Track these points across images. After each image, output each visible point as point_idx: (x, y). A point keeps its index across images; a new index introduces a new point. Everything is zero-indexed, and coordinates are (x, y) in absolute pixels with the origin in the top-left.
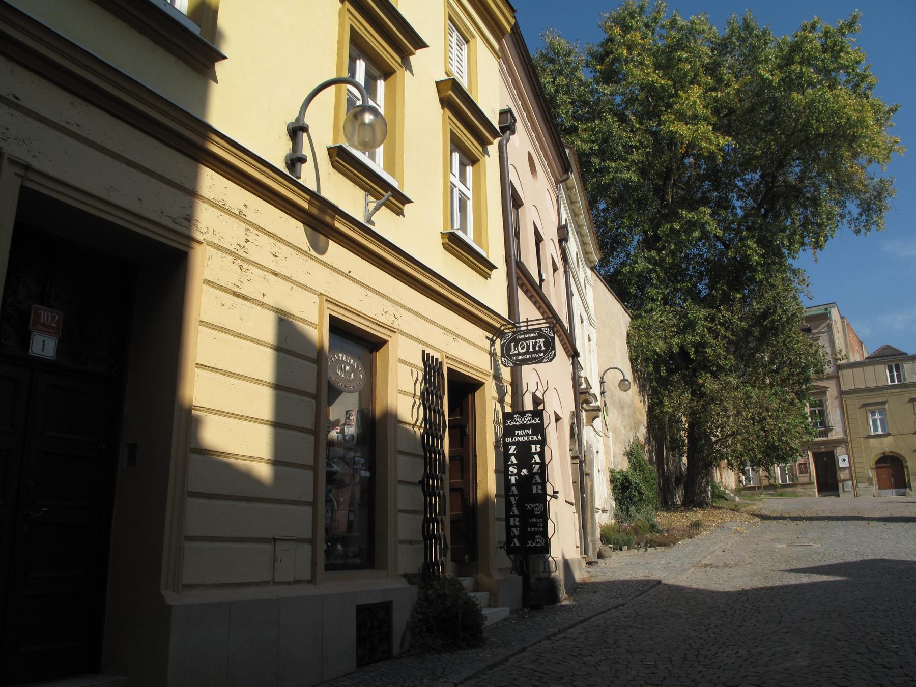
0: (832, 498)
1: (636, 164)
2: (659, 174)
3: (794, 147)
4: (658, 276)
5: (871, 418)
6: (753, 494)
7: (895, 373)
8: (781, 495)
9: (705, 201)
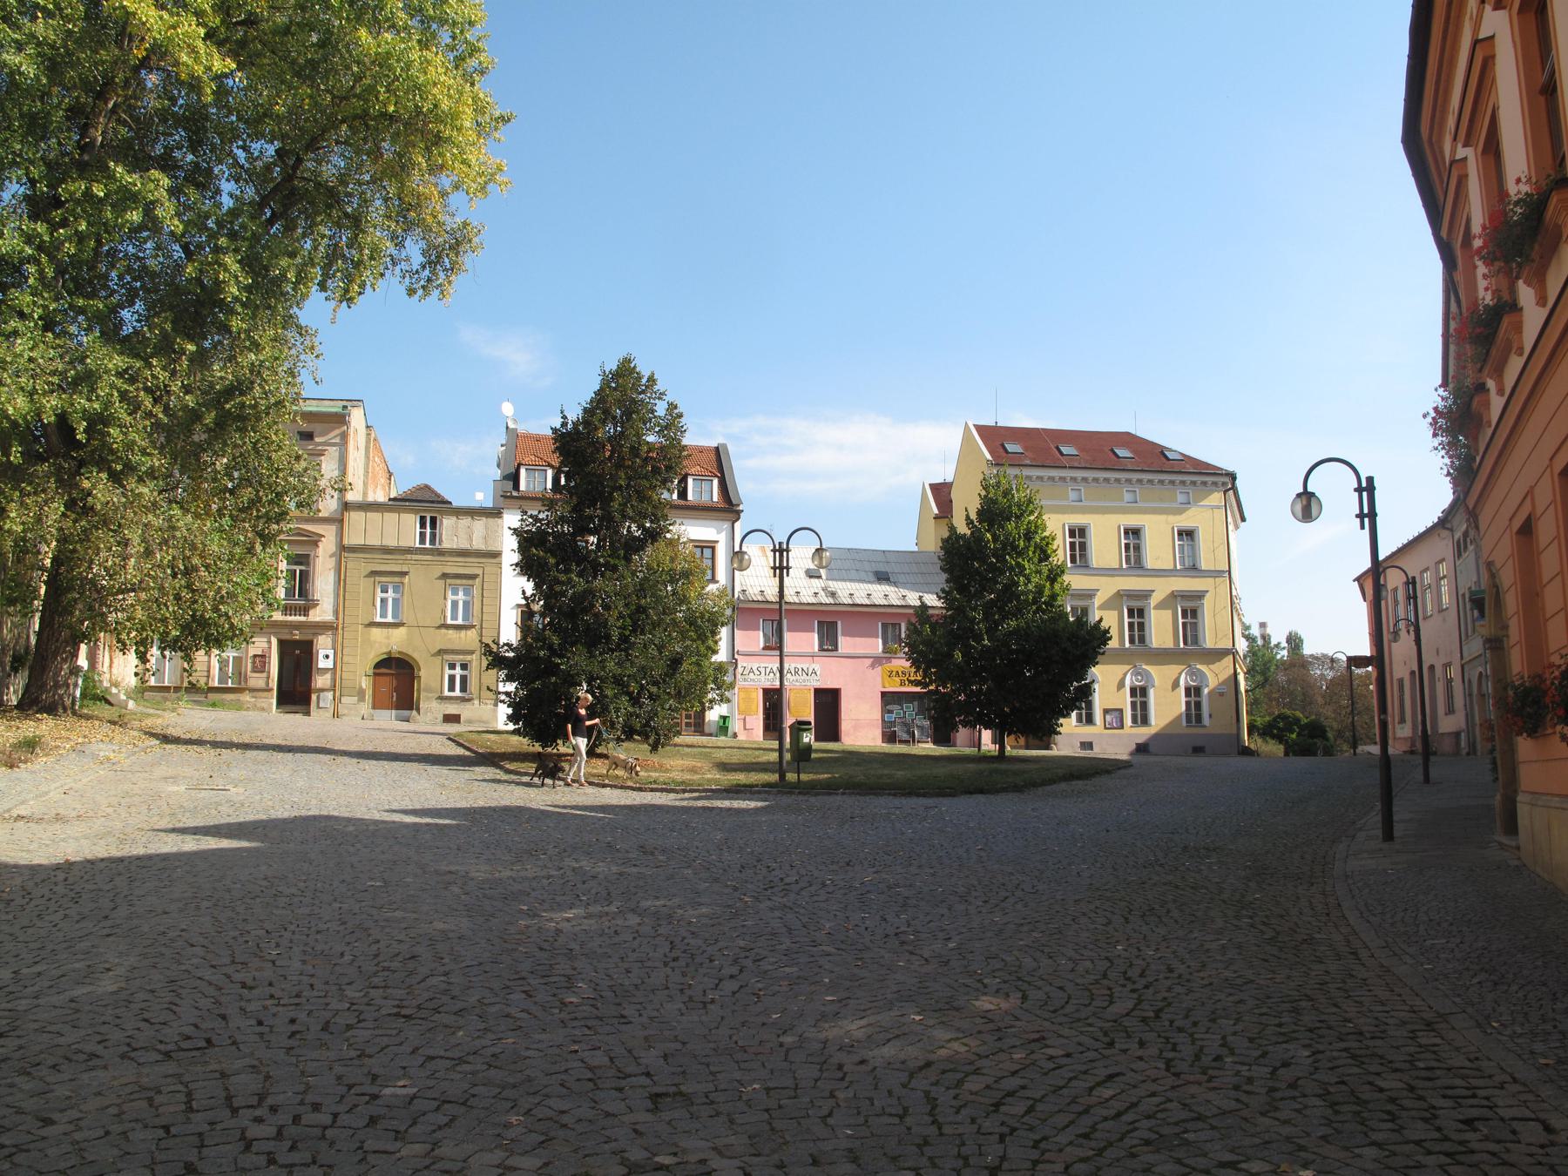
0: (299, 717)
1: (39, 44)
2: (86, 86)
3: (343, 121)
4: (41, 272)
5: (380, 595)
6: (166, 699)
7: (428, 530)
8: (214, 705)
9: (167, 164)
